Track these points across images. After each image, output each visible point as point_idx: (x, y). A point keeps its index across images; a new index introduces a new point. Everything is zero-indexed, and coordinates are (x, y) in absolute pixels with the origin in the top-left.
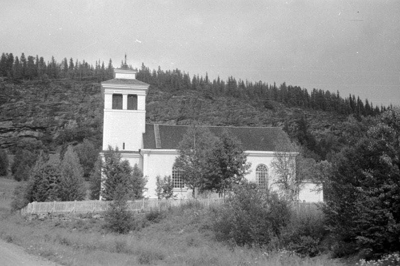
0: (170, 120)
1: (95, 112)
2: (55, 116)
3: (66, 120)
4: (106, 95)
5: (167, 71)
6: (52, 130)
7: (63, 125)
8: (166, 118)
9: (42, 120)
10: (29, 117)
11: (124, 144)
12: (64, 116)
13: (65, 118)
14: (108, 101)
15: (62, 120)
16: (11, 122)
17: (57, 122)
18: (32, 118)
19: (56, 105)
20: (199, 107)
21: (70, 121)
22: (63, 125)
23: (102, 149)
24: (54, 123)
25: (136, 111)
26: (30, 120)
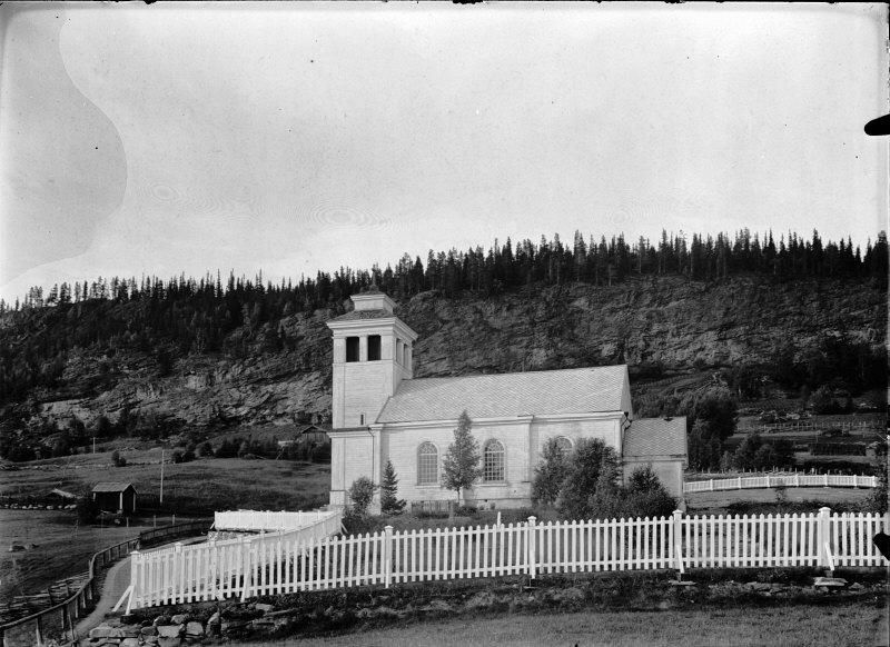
12: (525, 343)
14: (339, 346)
17: (515, 355)
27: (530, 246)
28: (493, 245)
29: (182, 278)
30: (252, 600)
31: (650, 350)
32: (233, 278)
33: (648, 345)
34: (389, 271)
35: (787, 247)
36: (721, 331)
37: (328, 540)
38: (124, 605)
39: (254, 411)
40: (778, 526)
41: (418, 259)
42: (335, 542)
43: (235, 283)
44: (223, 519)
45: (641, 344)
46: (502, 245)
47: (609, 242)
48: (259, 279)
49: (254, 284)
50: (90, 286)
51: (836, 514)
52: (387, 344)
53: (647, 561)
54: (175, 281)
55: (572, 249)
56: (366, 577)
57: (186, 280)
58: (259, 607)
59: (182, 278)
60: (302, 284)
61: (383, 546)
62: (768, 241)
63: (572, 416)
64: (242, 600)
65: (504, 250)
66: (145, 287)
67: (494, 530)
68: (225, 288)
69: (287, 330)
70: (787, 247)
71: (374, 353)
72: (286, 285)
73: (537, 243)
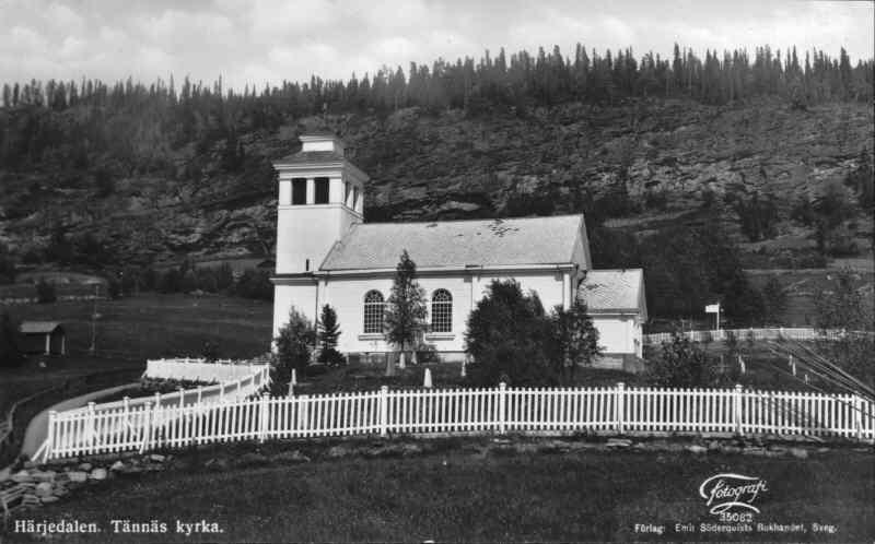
0: (718, 160)
1: (572, 157)
2: (499, 170)
3: (519, 177)
4: (281, 183)
5: (620, 53)
6: (495, 197)
7: (513, 187)
8: (709, 157)
9: (475, 181)
10: (452, 177)
11: (308, 262)
12: (514, 169)
13: (517, 173)
14: (285, 190)
15: (510, 178)
16: (424, 189)
17: (502, 182)
18: (459, 178)
19: (501, 150)
20: (777, 129)
21: (526, 178)
22: (513, 187)
23: (274, 271)
24: (496, 183)
25: (325, 206)
26: (457, 182)
27: (524, 55)
28: (484, 56)
29: (129, 84)
30: (150, 452)
31: (655, 179)
32: (188, 84)
33: (653, 174)
34: (366, 81)
35: (812, 66)
36: (735, 160)
37: (241, 400)
38: (40, 458)
39: (207, 239)
40: (596, 398)
41: (400, 68)
42: (248, 403)
43: (191, 89)
44: (157, 369)
45: (646, 172)
46: (494, 56)
47: (615, 56)
48: (218, 87)
49: (212, 91)
50: (21, 90)
51: (510, 389)
52: (336, 188)
53: (473, 425)
54: (122, 85)
55: (573, 62)
56: (246, 434)
57: (134, 84)
58: (154, 457)
59: (129, 84)
60: (267, 91)
61: (300, 409)
62: (792, 60)
63: (535, 267)
64: (141, 452)
65: (496, 61)
66: (86, 93)
67: (287, 401)
68: (179, 92)
69: (247, 149)
70: (812, 66)
71: (322, 196)
72: (250, 92)
73: (534, 54)
